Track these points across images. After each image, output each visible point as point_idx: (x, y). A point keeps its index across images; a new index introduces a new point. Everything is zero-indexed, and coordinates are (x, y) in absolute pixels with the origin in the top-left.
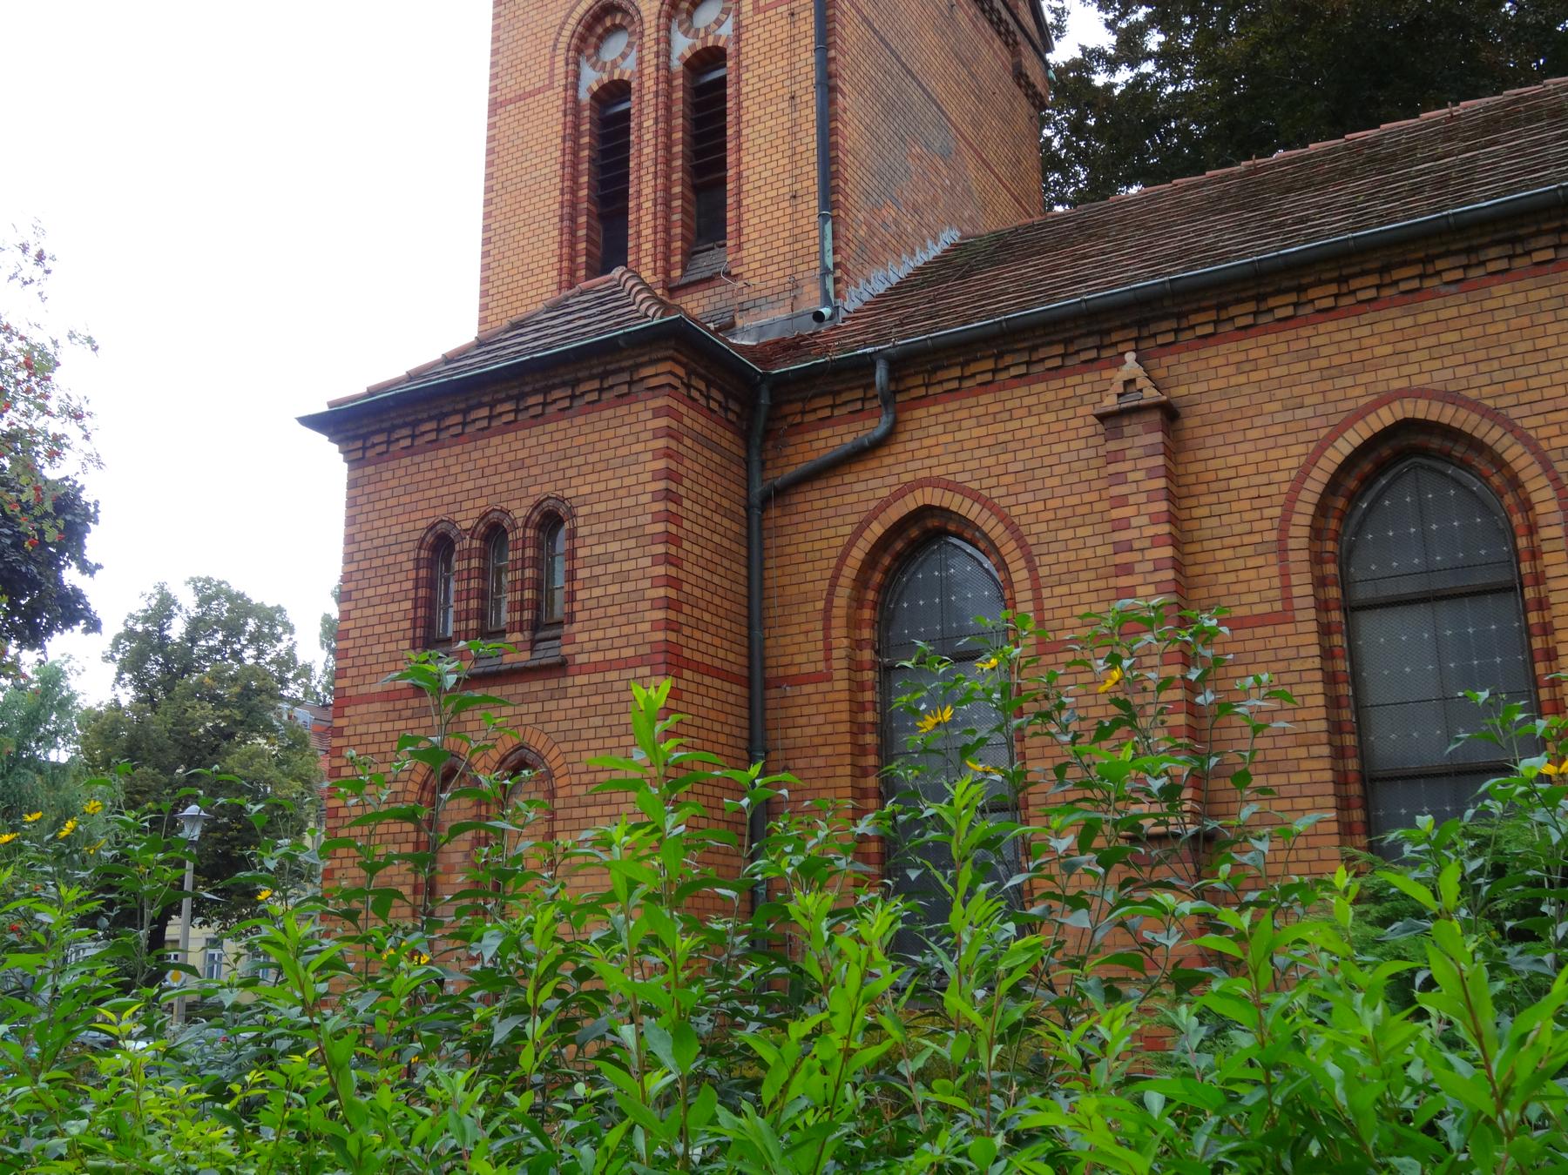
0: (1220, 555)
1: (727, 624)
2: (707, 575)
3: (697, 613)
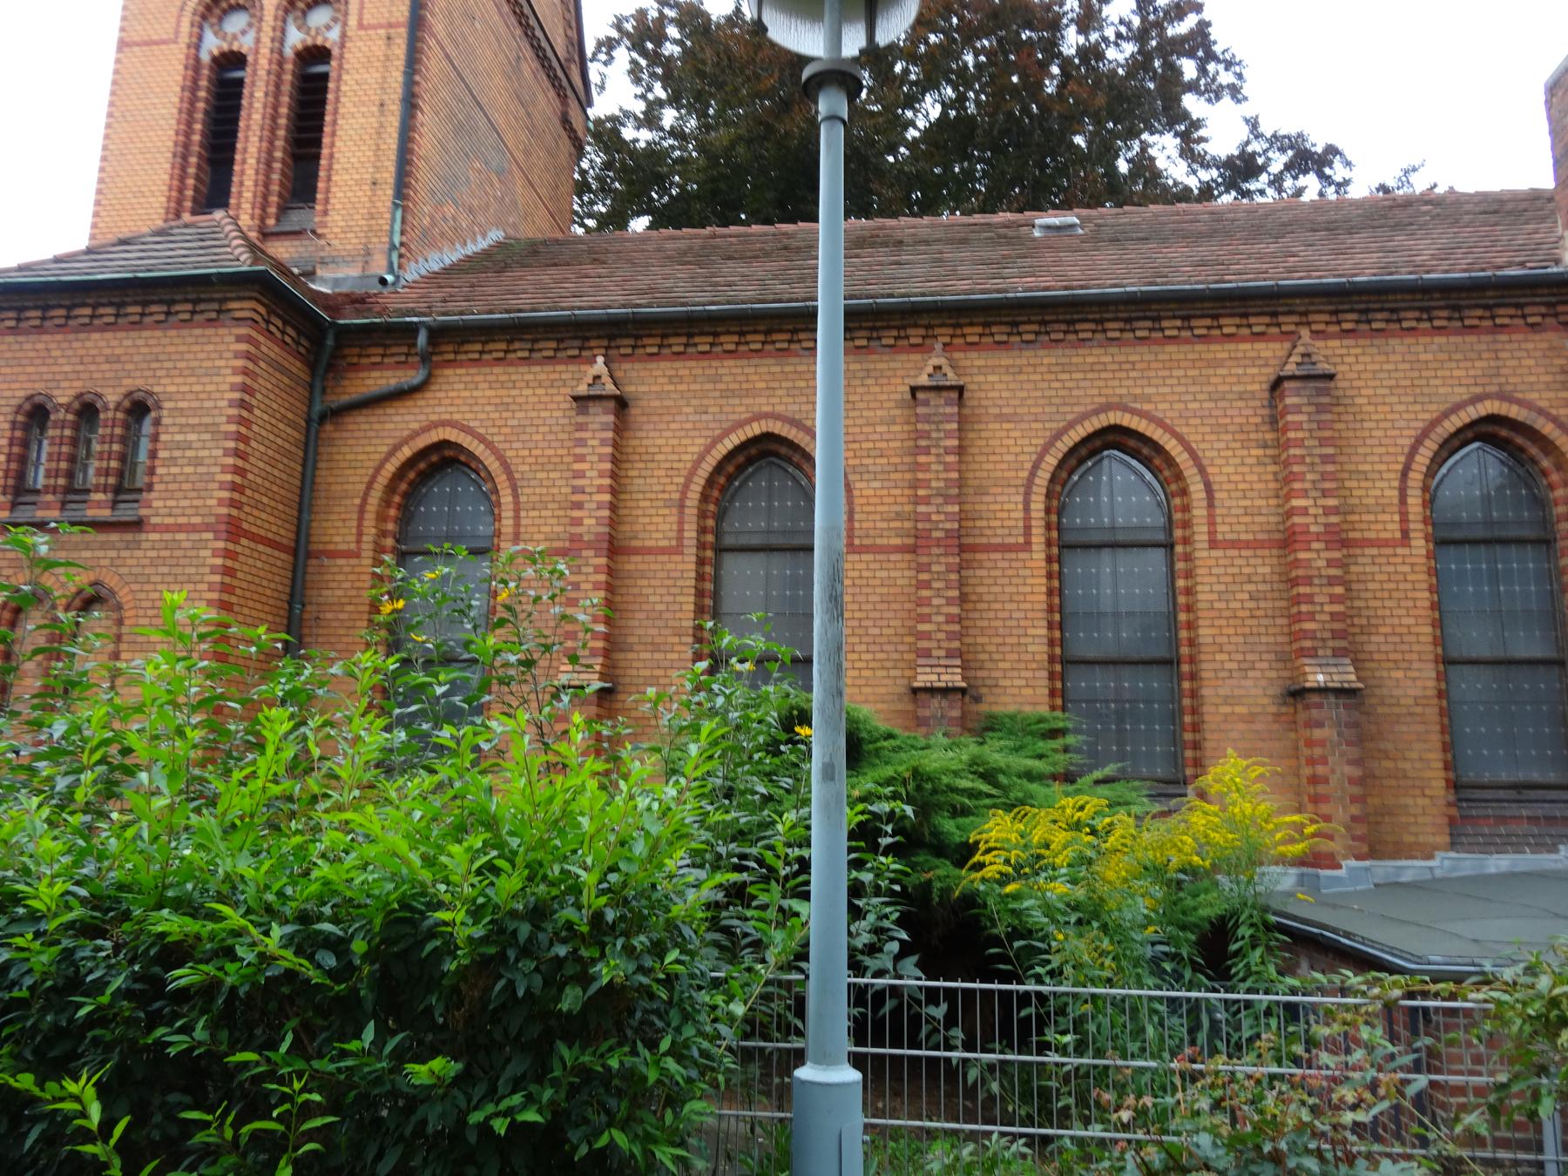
1: (281, 507)
2: (268, 469)
3: (257, 496)
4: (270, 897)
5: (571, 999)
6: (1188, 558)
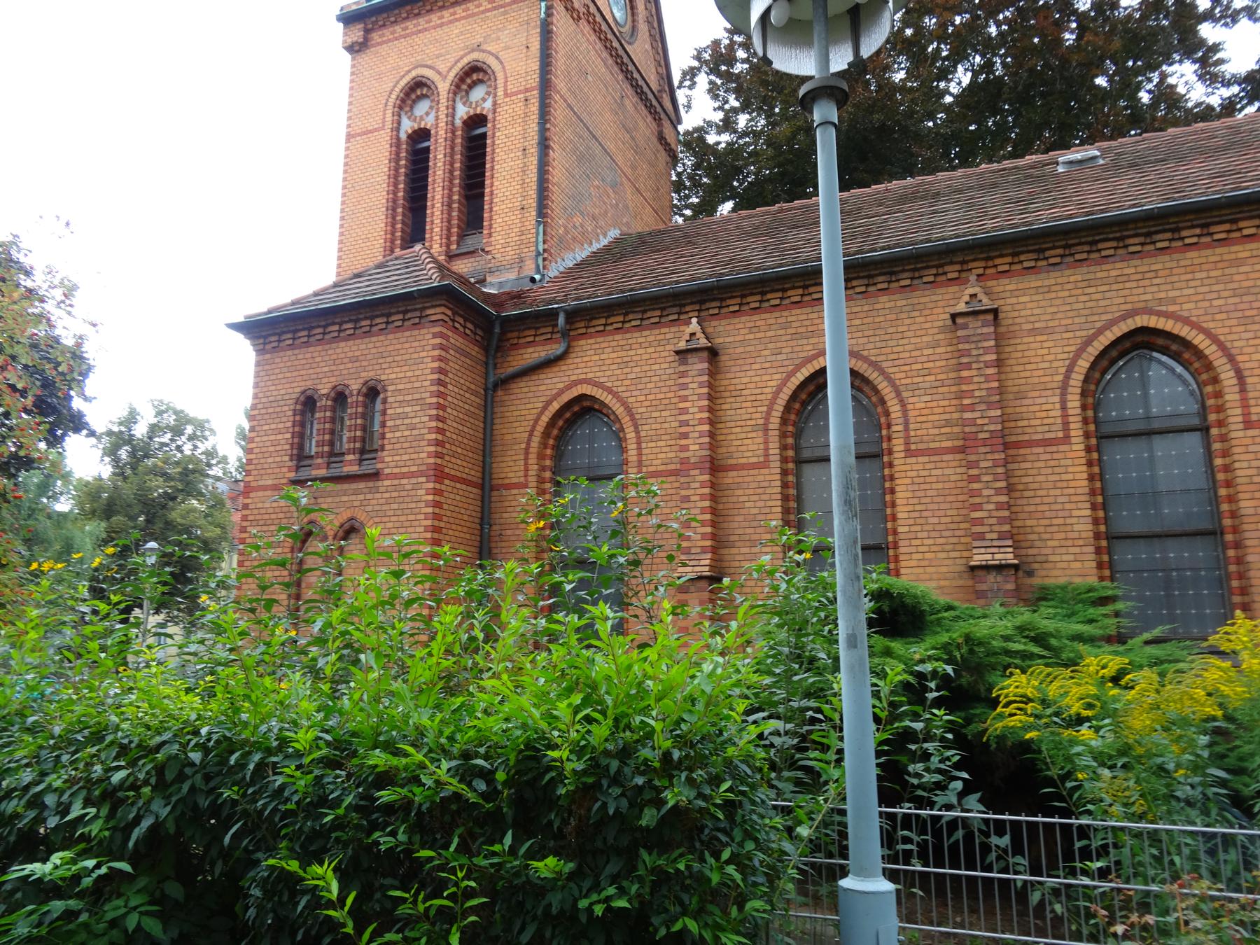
0: (734, 430)
1: (470, 454)
2: (460, 427)
3: (454, 448)
4: (443, 740)
5: (648, 818)
6: (1224, 438)
